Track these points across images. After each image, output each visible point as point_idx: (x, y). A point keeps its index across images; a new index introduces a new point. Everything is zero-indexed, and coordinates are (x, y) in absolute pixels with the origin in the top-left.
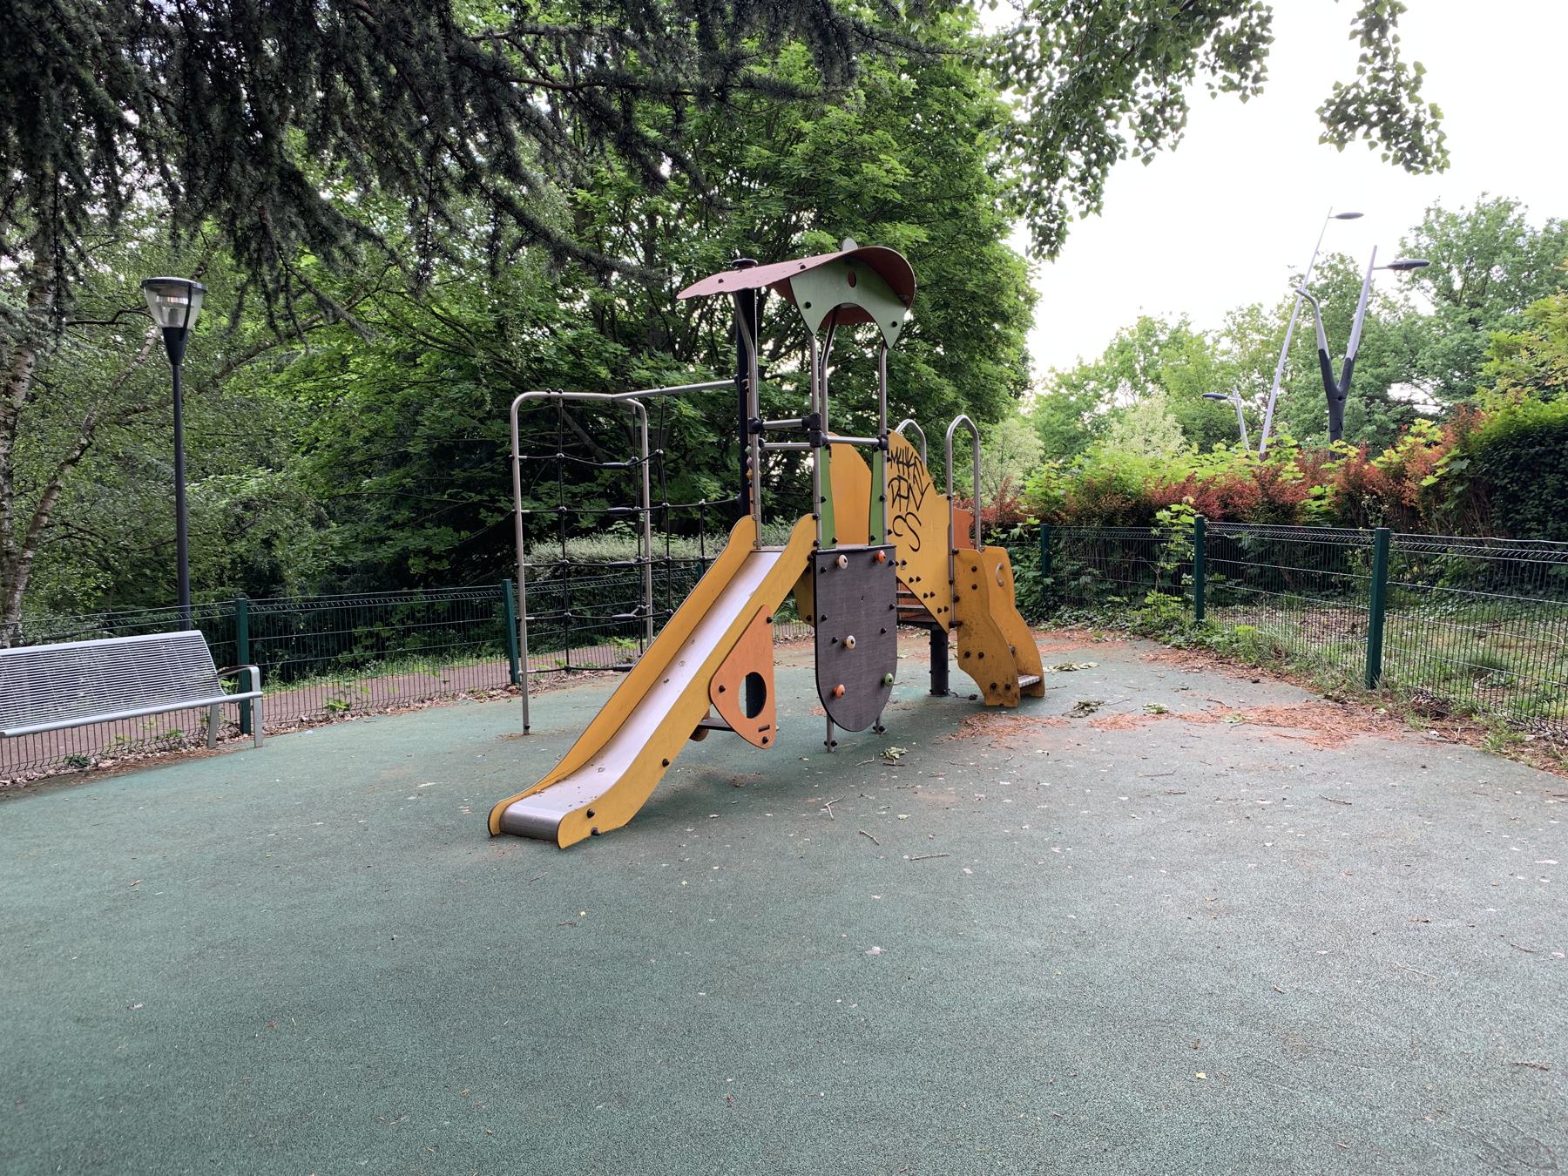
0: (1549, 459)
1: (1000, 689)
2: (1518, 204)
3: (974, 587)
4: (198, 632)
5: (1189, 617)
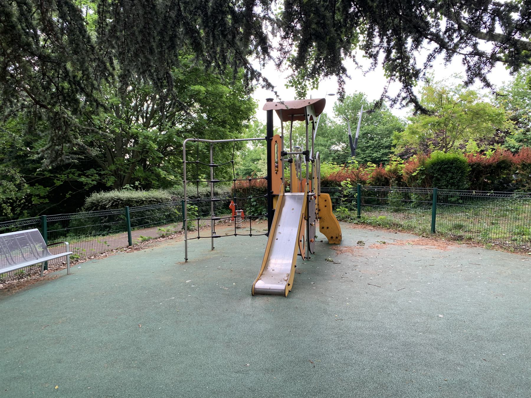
0: (449, 169)
1: (334, 238)
2: (365, 95)
3: (326, 206)
4: (37, 229)
5: (355, 214)
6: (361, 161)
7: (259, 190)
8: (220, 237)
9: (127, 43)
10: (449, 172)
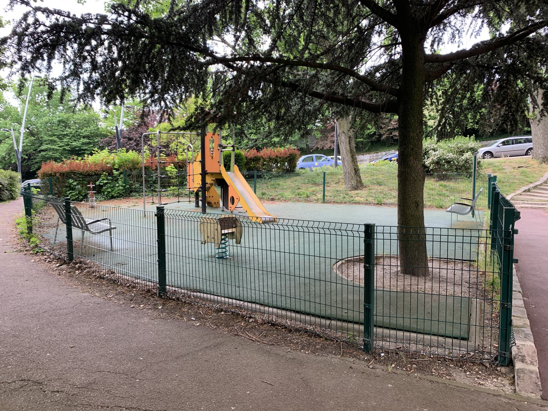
7: (81, 174)
8: (167, 204)
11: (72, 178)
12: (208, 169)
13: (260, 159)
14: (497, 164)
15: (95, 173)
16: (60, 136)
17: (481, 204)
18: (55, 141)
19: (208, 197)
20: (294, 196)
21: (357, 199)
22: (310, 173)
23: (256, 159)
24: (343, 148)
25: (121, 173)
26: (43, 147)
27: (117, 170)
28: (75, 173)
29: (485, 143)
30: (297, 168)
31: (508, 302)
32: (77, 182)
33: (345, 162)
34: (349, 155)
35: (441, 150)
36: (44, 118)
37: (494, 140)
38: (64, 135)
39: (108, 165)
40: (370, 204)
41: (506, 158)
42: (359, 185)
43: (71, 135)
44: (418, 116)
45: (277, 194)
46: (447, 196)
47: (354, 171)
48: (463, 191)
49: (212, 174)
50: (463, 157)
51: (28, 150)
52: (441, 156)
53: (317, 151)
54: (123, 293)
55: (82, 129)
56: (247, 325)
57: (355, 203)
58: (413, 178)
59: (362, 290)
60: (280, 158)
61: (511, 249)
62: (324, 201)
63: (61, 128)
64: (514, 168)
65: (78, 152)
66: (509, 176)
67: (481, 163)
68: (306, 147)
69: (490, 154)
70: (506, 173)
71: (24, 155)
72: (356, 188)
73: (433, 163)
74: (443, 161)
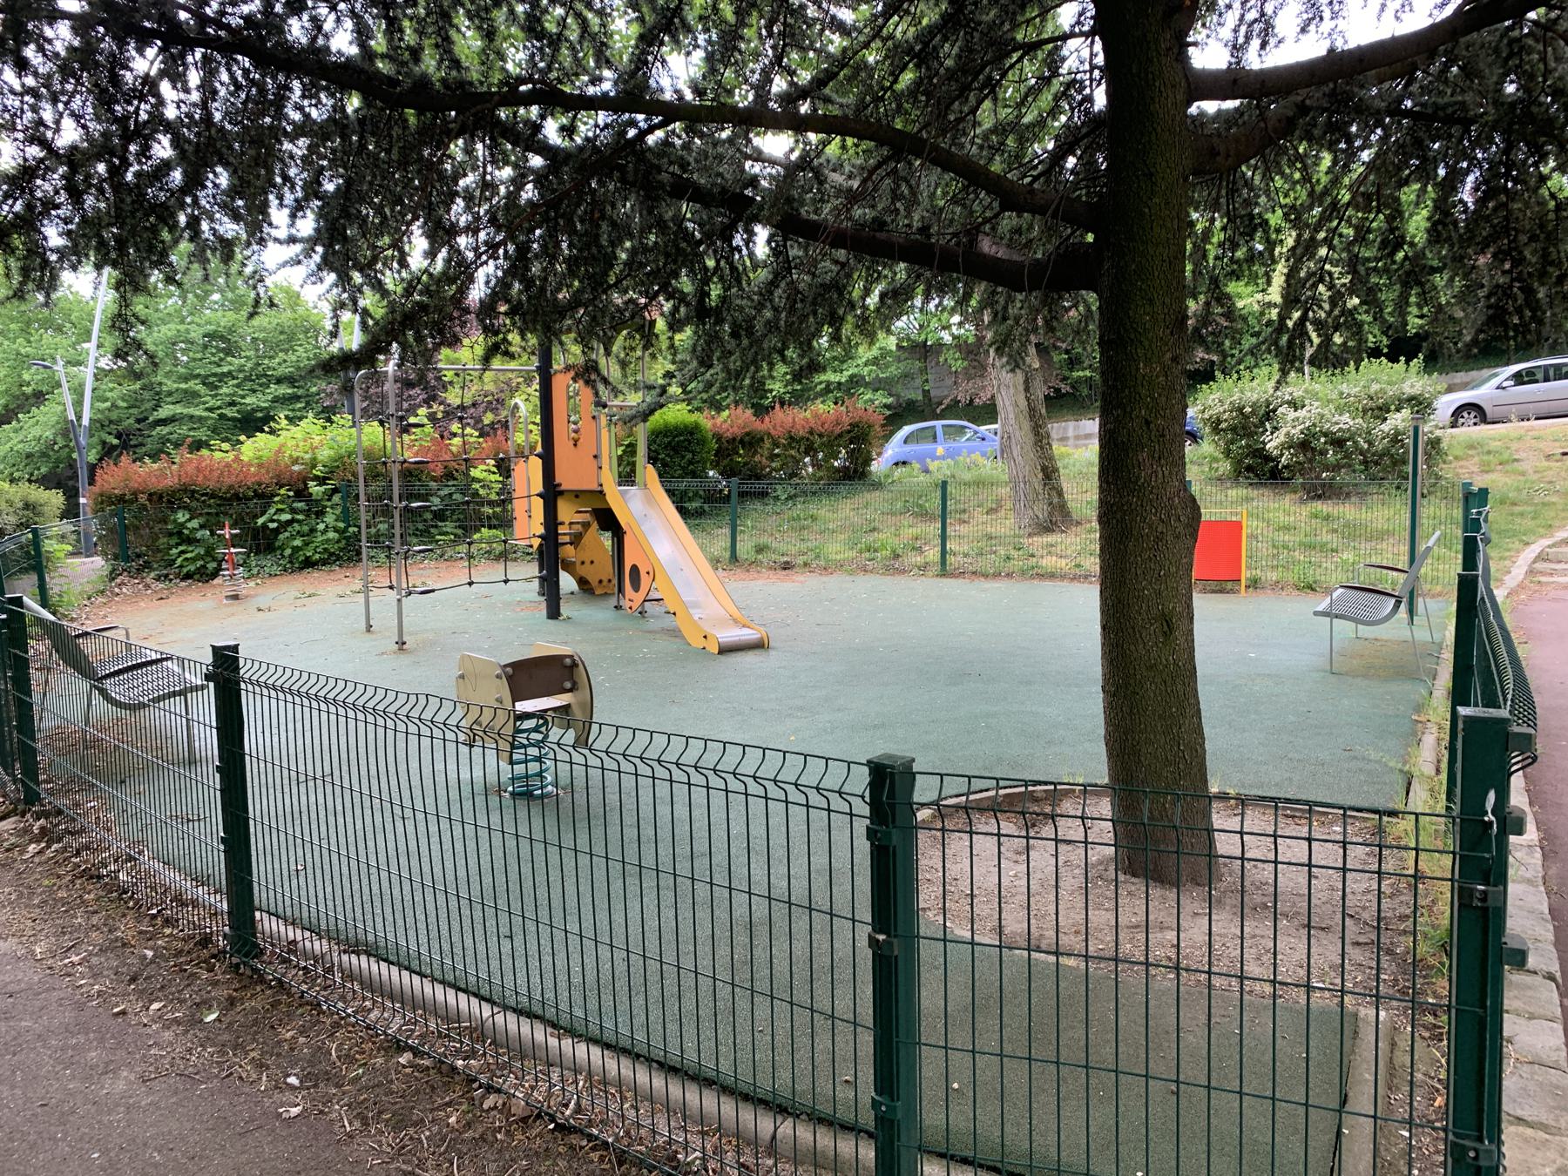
6: (207, 418)
7: (213, 496)
8: (433, 591)
9: (1473, 456)
10: (686, 449)
11: (186, 508)
12: (566, 478)
13: (762, 440)
14: (1494, 445)
15: (255, 491)
16: (211, 379)
17: (1441, 574)
18: (196, 394)
19: (578, 564)
20: (853, 554)
21: (1049, 562)
22: (922, 478)
23: (751, 441)
24: (1007, 403)
25: (335, 491)
26: (165, 412)
27: (321, 481)
28: (194, 492)
29: (1460, 377)
30: (877, 467)
31: (1480, 1139)
32: (202, 520)
33: (1013, 447)
34: (1027, 425)
35: (1316, 404)
36: (164, 329)
37: (1490, 367)
38: (223, 374)
39: (296, 468)
40: (1086, 577)
41: (1526, 423)
42: (1057, 517)
43: (241, 376)
44: (1167, 300)
45: (803, 547)
46: (1332, 551)
47: (1040, 475)
48: (1382, 535)
49: (577, 494)
50: (1386, 427)
51: (119, 421)
52: (1314, 425)
53: (953, 410)
54: (124, 945)
55: (271, 358)
56: (469, 1125)
57: (1041, 576)
58: (1150, 527)
59: (867, 1040)
60: (821, 436)
61: (1490, 903)
62: (944, 570)
63: (213, 354)
64: (1548, 457)
65: (253, 423)
66: (1533, 482)
67: (1444, 445)
68: (920, 398)
69: (1477, 411)
70: (1523, 474)
71: (110, 434)
72: (1047, 528)
73: (1289, 445)
74: (1322, 440)
